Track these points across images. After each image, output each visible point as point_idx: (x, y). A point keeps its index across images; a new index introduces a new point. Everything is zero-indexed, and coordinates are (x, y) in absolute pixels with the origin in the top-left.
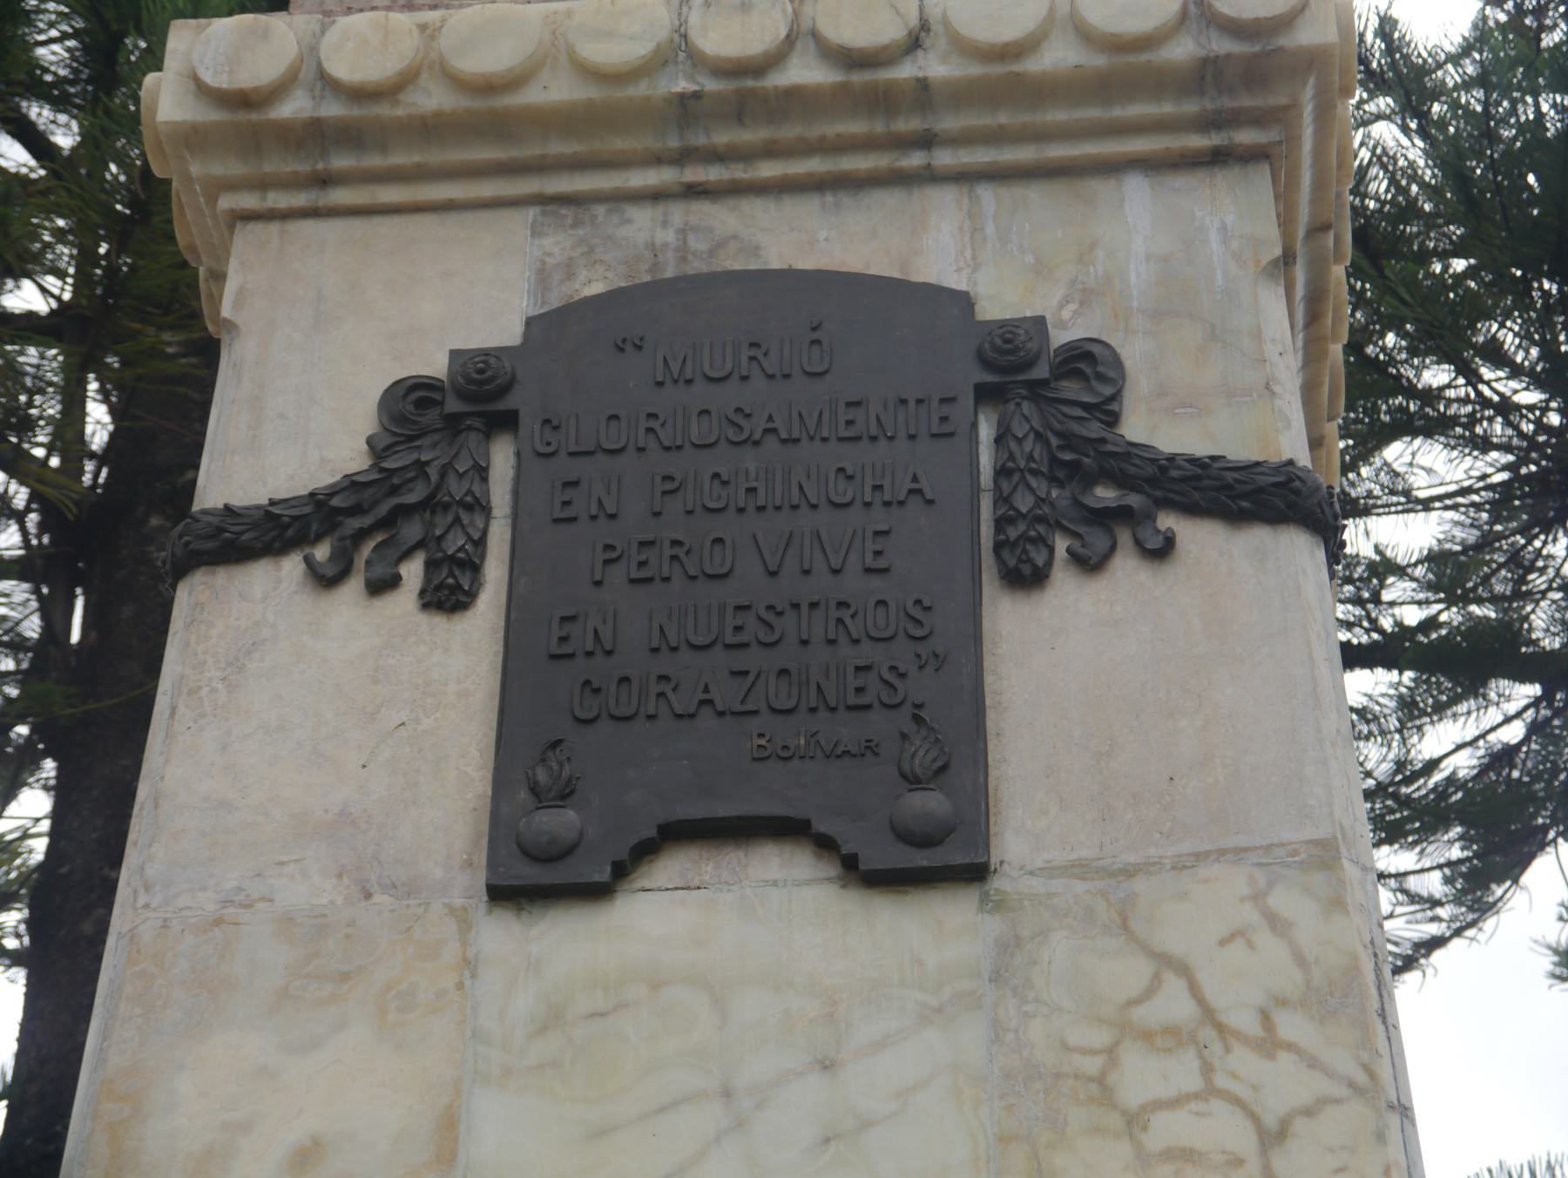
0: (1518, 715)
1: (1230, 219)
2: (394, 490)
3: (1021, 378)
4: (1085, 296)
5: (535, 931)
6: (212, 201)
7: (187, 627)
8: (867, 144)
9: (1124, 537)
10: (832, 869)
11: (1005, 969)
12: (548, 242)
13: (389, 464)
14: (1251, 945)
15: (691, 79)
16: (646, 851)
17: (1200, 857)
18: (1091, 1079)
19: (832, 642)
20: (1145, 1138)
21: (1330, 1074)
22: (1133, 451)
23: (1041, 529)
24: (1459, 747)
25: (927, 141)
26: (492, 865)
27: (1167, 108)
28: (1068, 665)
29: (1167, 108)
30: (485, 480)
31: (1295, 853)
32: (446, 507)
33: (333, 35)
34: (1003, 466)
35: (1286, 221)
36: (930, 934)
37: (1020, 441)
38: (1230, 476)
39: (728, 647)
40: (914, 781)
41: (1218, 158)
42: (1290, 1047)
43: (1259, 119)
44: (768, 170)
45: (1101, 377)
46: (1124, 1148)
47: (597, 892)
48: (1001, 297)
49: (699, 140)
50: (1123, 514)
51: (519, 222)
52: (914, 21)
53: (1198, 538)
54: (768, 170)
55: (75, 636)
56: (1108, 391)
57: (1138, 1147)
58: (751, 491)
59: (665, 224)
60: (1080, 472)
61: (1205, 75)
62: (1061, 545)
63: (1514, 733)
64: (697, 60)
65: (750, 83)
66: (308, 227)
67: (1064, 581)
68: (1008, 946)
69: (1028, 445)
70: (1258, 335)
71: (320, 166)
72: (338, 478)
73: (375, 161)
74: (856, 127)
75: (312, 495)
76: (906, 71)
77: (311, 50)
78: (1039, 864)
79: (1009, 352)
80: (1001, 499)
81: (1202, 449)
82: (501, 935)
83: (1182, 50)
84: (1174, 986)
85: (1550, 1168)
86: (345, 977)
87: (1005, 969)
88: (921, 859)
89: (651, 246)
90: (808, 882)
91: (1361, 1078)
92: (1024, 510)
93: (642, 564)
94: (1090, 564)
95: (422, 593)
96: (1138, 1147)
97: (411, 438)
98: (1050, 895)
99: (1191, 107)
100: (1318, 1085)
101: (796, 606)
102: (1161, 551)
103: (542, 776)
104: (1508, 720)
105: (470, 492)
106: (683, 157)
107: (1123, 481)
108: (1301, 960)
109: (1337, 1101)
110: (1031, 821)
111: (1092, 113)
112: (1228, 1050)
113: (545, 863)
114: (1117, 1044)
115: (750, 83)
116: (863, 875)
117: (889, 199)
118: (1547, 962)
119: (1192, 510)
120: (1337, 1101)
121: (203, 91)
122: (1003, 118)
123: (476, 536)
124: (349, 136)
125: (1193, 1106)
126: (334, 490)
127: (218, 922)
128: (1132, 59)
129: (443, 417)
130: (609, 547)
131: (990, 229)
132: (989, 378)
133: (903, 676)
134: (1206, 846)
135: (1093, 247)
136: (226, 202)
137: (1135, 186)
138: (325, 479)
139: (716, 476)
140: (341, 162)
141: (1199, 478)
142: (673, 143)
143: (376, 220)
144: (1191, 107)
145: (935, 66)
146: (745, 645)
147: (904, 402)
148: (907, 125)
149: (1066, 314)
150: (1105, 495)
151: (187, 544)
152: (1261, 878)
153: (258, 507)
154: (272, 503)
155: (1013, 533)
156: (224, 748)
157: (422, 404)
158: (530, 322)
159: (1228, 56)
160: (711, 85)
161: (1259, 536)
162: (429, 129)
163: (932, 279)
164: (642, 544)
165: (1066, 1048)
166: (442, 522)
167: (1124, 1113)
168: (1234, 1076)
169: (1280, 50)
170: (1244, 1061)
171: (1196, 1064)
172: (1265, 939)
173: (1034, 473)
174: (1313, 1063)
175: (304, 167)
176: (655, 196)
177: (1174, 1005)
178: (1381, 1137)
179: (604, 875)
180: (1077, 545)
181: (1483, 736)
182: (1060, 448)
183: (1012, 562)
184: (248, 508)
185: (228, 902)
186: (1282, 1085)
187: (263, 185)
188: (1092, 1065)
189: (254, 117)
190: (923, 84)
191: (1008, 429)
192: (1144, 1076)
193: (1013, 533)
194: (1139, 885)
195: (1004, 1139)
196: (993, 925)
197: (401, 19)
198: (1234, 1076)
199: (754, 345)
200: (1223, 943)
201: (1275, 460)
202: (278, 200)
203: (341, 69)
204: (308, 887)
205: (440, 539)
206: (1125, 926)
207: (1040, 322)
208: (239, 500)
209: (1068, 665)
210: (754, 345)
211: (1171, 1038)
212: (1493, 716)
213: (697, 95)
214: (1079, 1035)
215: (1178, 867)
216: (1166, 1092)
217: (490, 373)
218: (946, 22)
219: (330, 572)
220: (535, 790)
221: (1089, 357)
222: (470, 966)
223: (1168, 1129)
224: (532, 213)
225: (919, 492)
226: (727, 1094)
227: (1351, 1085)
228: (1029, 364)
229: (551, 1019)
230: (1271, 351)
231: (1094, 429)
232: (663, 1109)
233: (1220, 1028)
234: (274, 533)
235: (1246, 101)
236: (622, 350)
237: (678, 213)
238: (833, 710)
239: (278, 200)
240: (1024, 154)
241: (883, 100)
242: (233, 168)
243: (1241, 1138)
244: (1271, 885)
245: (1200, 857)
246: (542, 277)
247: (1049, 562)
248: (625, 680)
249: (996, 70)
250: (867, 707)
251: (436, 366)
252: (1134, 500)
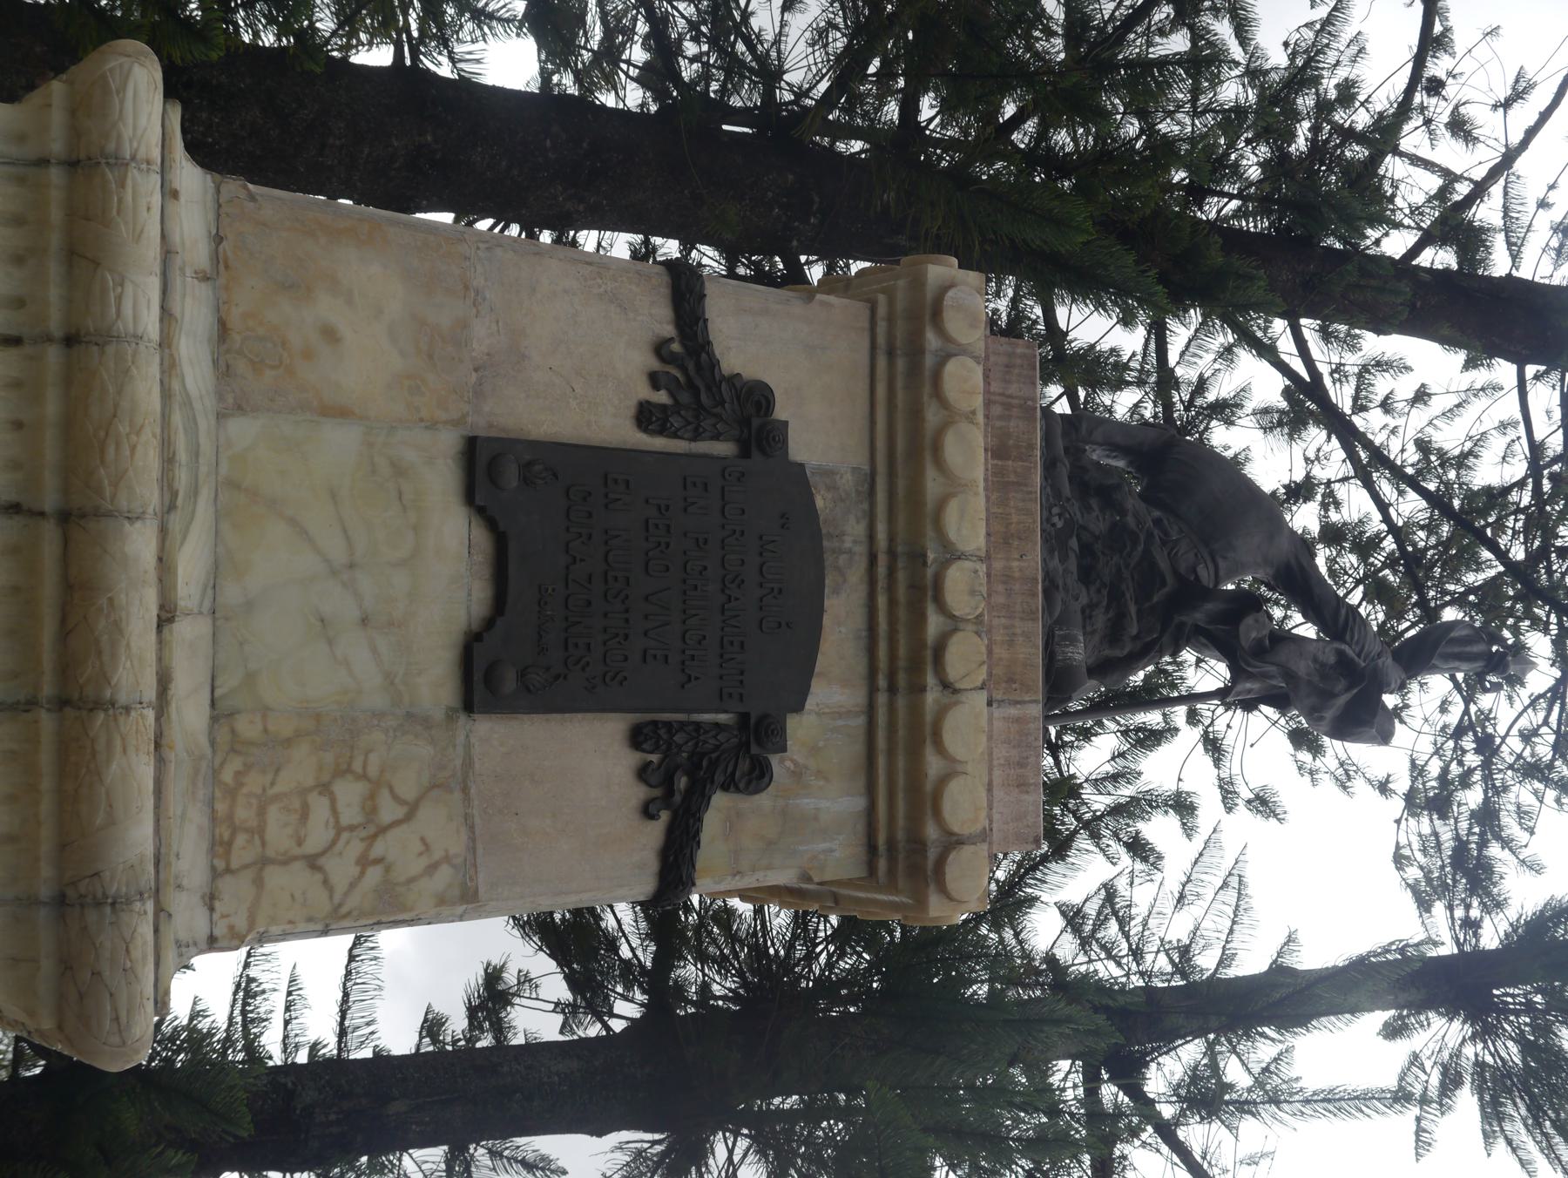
0: (635, 955)
1: (837, 854)
2: (709, 388)
4: (797, 774)
5: (450, 461)
6: (883, 291)
7: (638, 272)
8: (893, 657)
9: (657, 792)
10: (475, 627)
11: (414, 720)
12: (849, 476)
13: (724, 386)
14: (421, 854)
15: (935, 560)
16: (491, 524)
17: (472, 828)
18: (349, 765)
19: (605, 631)
20: (315, 793)
21: (346, 894)
22: (706, 801)
24: (618, 921)
25: (892, 689)
26: (489, 439)
27: (901, 822)
28: (587, 762)
29: (901, 822)
30: (712, 438)
31: (471, 880)
33: (970, 362)
35: (839, 883)
36: (436, 681)
37: (715, 737)
39: (606, 573)
40: (522, 674)
41: (872, 848)
42: (362, 873)
43: (891, 872)
44: (882, 601)
45: (749, 783)
46: (310, 782)
47: (470, 496)
48: (800, 729)
49: (901, 564)
50: (670, 792)
51: (860, 460)
52: (958, 686)
53: (653, 834)
54: (882, 601)
55: (725, 127)
56: (742, 786)
57: (311, 789)
58: (696, 588)
59: (855, 542)
60: (697, 768)
61: (917, 844)
62: (655, 758)
63: (625, 952)
64: (945, 564)
65: (930, 593)
66: (865, 343)
67: (632, 759)
68: (427, 722)
69: (712, 741)
70: (769, 867)
72: (718, 356)
73: (900, 383)
74: (902, 651)
75: (709, 343)
76: (931, 680)
77: (963, 351)
78: (473, 740)
80: (682, 725)
81: (705, 837)
82: (448, 442)
83: (931, 832)
84: (400, 812)
85: (376, 958)
86: (430, 357)
87: (414, 720)
88: (478, 676)
89: (843, 534)
90: (469, 613)
91: (344, 910)
93: (657, 526)
94: (642, 773)
95: (648, 402)
96: (311, 789)
97: (738, 398)
98: (454, 746)
99: (900, 835)
100: (340, 884)
101: (627, 611)
102: (648, 812)
103: (537, 468)
104: (633, 950)
106: (892, 554)
107: (689, 792)
108: (411, 880)
109: (331, 897)
110: (497, 738)
111: (901, 781)
112: (362, 840)
113: (493, 472)
114: (369, 780)
115: (930, 593)
117: (861, 667)
118: (496, 961)
119: (670, 831)
120: (331, 897)
121: (945, 289)
122: (901, 733)
124: (915, 369)
125: (332, 820)
126: (711, 355)
127: (466, 288)
128: (929, 805)
129: (750, 413)
130: (667, 508)
131: (840, 723)
132: (753, 721)
133: (583, 669)
134: (477, 831)
135: (827, 779)
136: (882, 298)
137: (859, 803)
138: (718, 351)
139: (705, 568)
140: (901, 364)
142: (900, 549)
143: (867, 381)
144: (900, 835)
145: (932, 696)
146: (606, 581)
147: (742, 673)
148: (902, 679)
149: (788, 763)
150: (682, 782)
152: (459, 861)
154: (706, 321)
155: (662, 732)
156: (566, 291)
157: (758, 405)
158: (802, 466)
159: (926, 858)
160: (930, 572)
161: (653, 865)
162: (916, 414)
163: (812, 689)
164: (668, 526)
165: (367, 753)
167: (330, 783)
168: (348, 843)
169: (927, 885)
170: (355, 848)
171: (355, 822)
172: (423, 862)
173: (696, 745)
174: (352, 886)
175: (899, 343)
176: (871, 537)
177: (389, 811)
178: (310, 919)
179: (479, 501)
181: (624, 935)
183: (645, 731)
185: (477, 292)
186: (341, 868)
187: (890, 319)
188: (357, 766)
189: (927, 317)
190: (923, 689)
192: (349, 793)
193: (662, 732)
194: (457, 795)
195: (318, 717)
196: (439, 715)
197: (978, 402)
198: (348, 843)
199: (780, 591)
200: (423, 839)
201: (696, 875)
202: (882, 327)
203: (951, 367)
204: (483, 337)
206: (433, 786)
207: (784, 749)
208: (708, 302)
209: (587, 762)
210: (780, 591)
211: (370, 808)
212: (635, 942)
213: (925, 564)
214: (374, 759)
215: (467, 817)
216: (340, 806)
218: (956, 703)
219: (664, 352)
220: (530, 464)
221: (762, 776)
222: (432, 425)
223: (320, 808)
224: (866, 468)
225: (689, 680)
226: (351, 566)
227: (340, 905)
228: (759, 743)
229: (399, 470)
230: (760, 875)
231: (719, 777)
232: (345, 531)
233: (374, 837)
235: (901, 866)
236: (782, 516)
237: (861, 549)
238: (566, 630)
239: (882, 327)
240: (881, 742)
241: (916, 667)
242: (900, 305)
243: (314, 843)
244: (454, 866)
245: (472, 828)
246: (829, 473)
247: (644, 751)
248: (590, 515)
249: (928, 730)
250: (566, 649)
251: (780, 413)
252: (678, 798)
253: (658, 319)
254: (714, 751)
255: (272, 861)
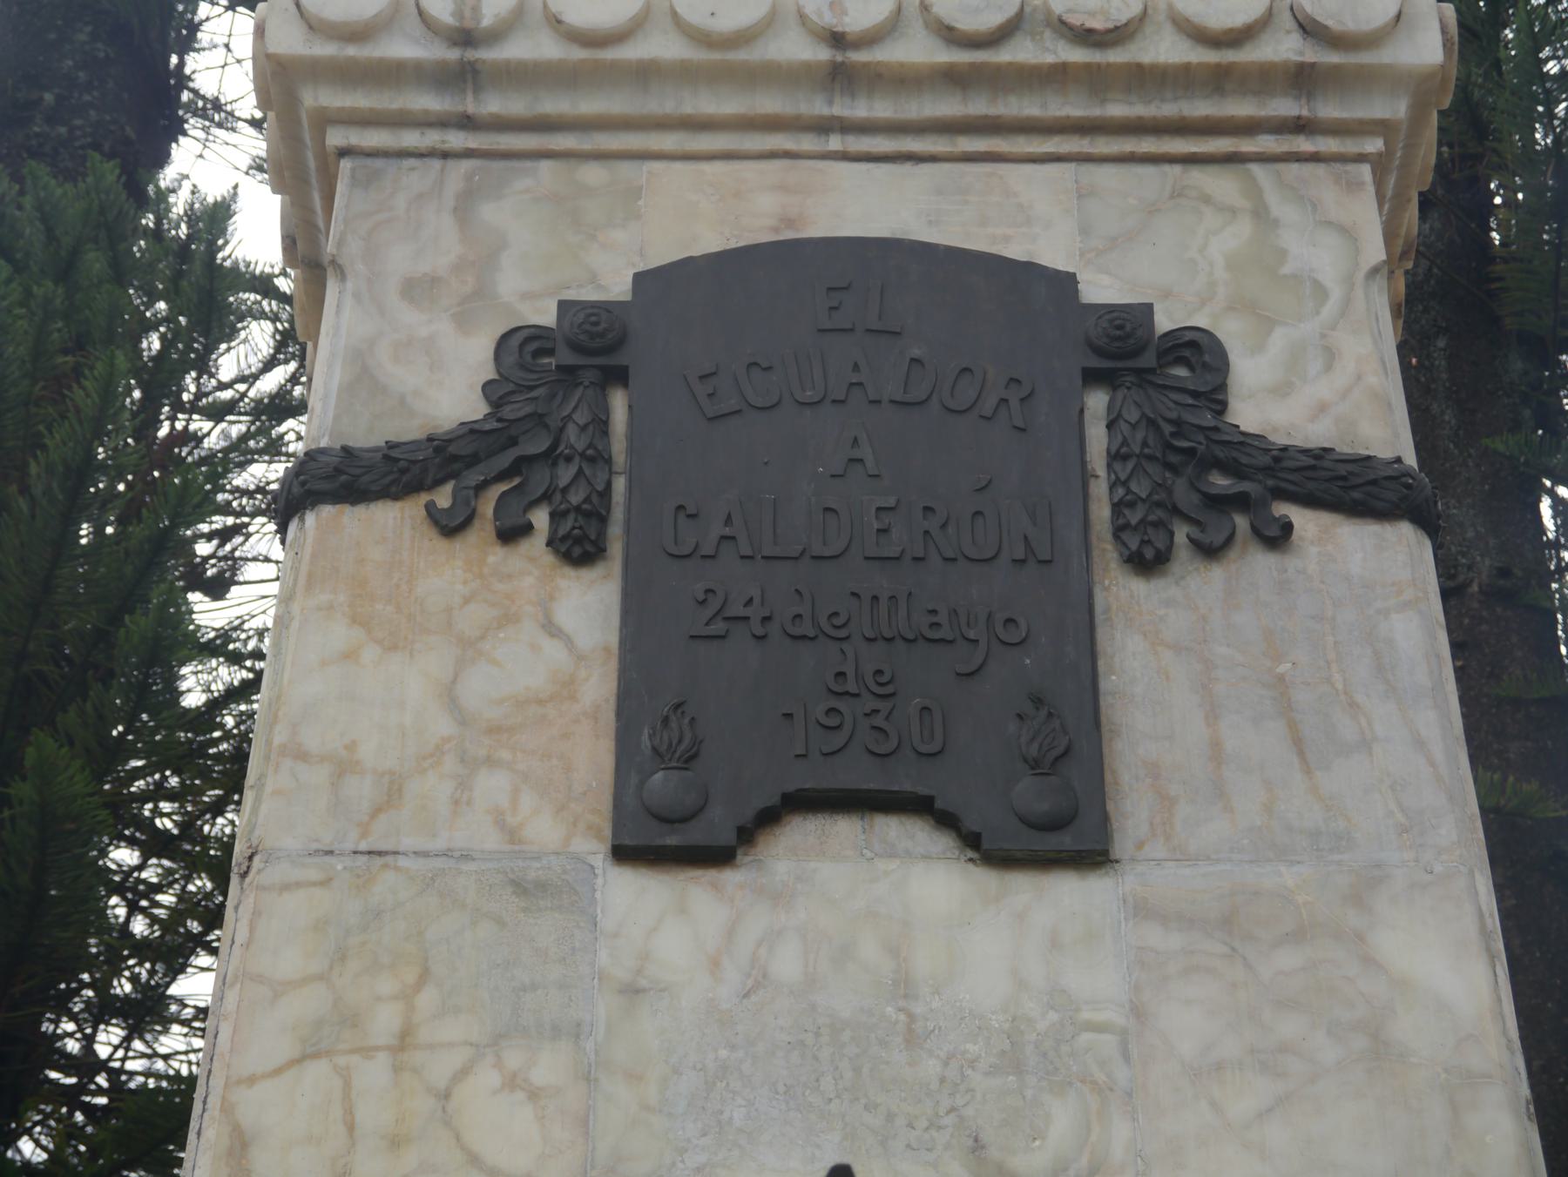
2: (513, 442)
3: (1129, 364)
8: (442, 122)
16: (769, 818)
22: (1249, 442)
23: (1159, 514)
32: (569, 459)
34: (1118, 451)
38: (1342, 470)
47: (716, 856)
49: (470, 106)
62: (1181, 533)
71: (1305, 113)
75: (430, 439)
79: (1119, 338)
92: (1144, 496)
94: (1210, 551)
102: (1278, 538)
105: (590, 446)
107: (1233, 469)
113: (681, 817)
116: (990, 849)
119: (1311, 501)
123: (600, 488)
136: (336, 138)
138: (1298, 441)
140: (1329, 110)
141: (1313, 468)
150: (1220, 482)
151: (303, 484)
153: (376, 450)
155: (1134, 517)
166: (565, 474)
173: (1150, 458)
179: (727, 837)
180: (1196, 534)
182: (1173, 435)
184: (361, 450)
191: (1119, 415)
193: (1134, 517)
205: (565, 490)
207: (1148, 309)
209: (1176, 653)
217: (603, 325)
231: (1208, 419)
234: (390, 478)
249: (716, 56)
253: (389, 524)
254: (1158, 428)
255: (239, 1082)
